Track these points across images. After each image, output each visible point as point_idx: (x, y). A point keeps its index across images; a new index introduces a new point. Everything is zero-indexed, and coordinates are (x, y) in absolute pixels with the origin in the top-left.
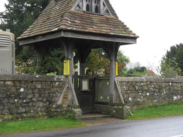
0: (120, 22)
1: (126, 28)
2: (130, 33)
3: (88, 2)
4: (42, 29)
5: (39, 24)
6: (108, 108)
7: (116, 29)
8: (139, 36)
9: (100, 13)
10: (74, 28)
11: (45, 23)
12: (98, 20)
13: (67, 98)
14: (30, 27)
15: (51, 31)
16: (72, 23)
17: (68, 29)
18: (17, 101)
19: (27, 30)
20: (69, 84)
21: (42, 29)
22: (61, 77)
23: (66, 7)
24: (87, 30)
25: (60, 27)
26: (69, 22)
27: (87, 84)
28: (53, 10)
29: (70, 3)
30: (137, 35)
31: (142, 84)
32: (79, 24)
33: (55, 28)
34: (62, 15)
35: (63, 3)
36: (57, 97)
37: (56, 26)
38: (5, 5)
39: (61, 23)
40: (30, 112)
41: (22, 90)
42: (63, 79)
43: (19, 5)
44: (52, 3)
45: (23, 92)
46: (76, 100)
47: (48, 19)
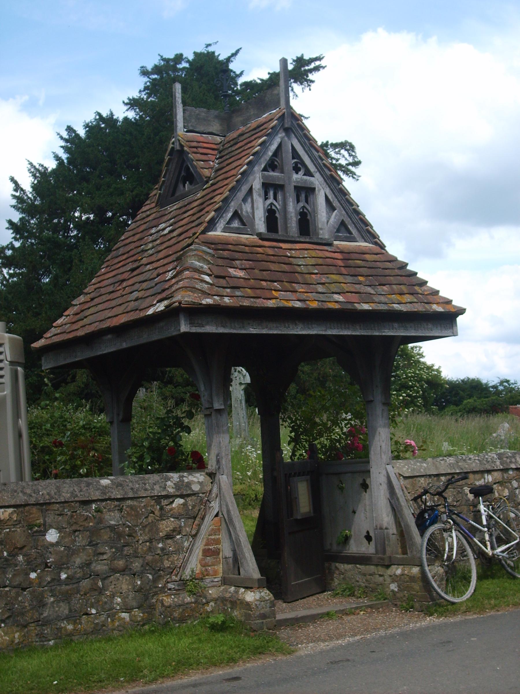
0: (393, 260)
1: (407, 273)
2: (431, 298)
3: (271, 200)
4: (113, 308)
5: (103, 291)
6: (370, 575)
7: (380, 289)
8: (464, 307)
9: (318, 234)
10: (226, 300)
11: (125, 284)
12: (312, 261)
13: (216, 553)
14: (74, 303)
15: (142, 314)
16: (216, 280)
17: (204, 302)
18: (39, 577)
19: (66, 313)
20: (221, 500)
21: (113, 308)
22: (191, 478)
23: (193, 224)
24: (274, 301)
25: (174, 300)
26: (207, 278)
27: (310, 225)
28: (151, 238)
29: (206, 210)
30: (457, 302)
31: (489, 478)
32: (242, 283)
33: (158, 302)
34: (179, 254)
35: (184, 209)
36: (177, 551)
37: (159, 297)
38: (10, 222)
39: (177, 283)
40: (87, 614)
41: (52, 536)
42: (201, 483)
43: (56, 221)
44: (148, 213)
45: (57, 544)
46: (249, 559)
47: (133, 270)
